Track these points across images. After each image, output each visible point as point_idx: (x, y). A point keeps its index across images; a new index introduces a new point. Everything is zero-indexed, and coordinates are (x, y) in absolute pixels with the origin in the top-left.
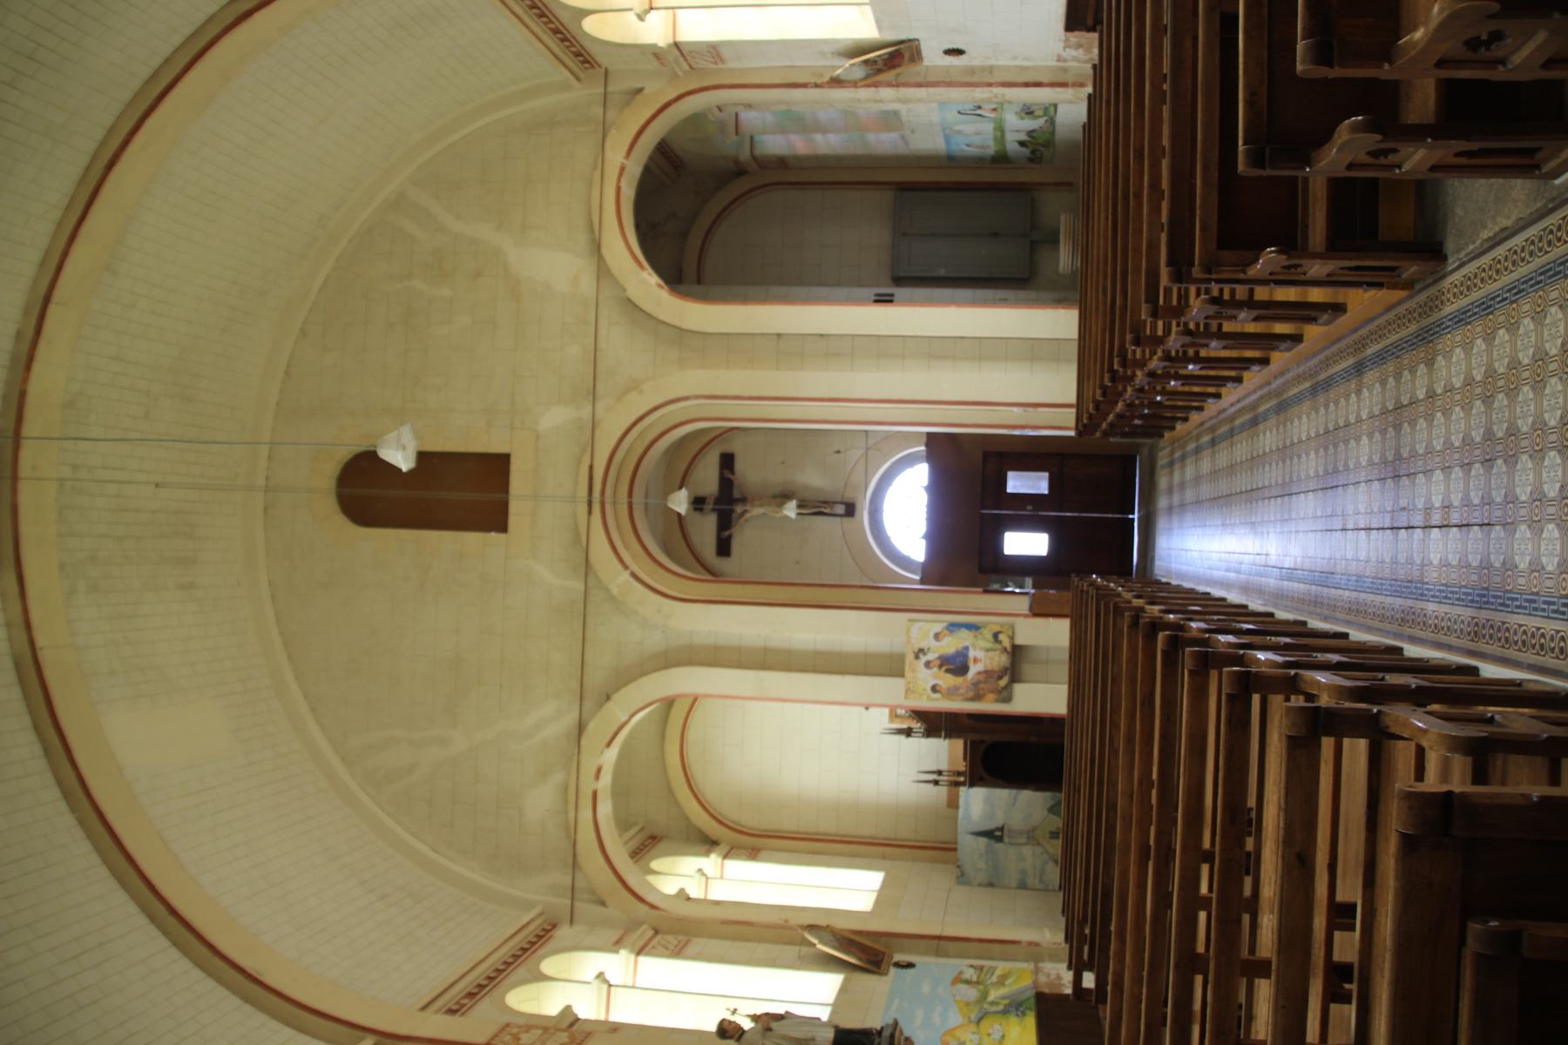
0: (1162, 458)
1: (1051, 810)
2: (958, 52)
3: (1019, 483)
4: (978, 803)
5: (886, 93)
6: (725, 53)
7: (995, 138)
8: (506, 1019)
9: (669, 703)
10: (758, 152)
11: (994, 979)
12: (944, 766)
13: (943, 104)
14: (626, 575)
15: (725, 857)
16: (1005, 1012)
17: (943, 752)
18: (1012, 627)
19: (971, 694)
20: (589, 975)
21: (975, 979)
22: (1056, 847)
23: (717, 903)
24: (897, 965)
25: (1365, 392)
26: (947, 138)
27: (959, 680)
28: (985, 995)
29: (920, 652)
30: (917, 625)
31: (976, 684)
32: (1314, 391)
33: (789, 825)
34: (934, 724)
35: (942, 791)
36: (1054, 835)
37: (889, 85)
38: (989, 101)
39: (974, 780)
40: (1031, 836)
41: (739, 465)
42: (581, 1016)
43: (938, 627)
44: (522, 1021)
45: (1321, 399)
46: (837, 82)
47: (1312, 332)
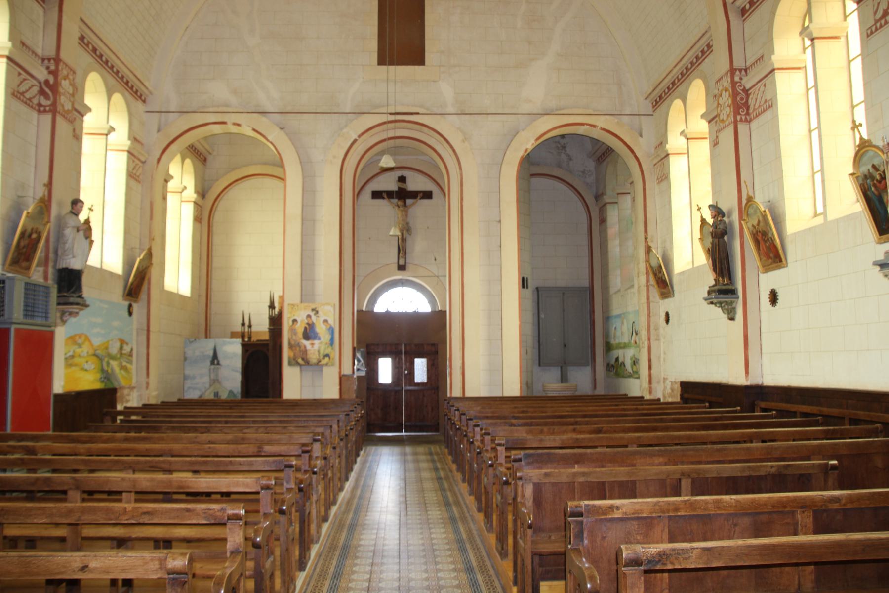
0: (434, 448)
1: (231, 392)
2: (667, 320)
3: (420, 367)
4: (233, 350)
5: (643, 279)
6: (664, 184)
7: (620, 344)
8: (79, 72)
9: (282, 165)
10: (609, 207)
11: (124, 364)
12: (254, 329)
13: (637, 313)
14: (355, 137)
15: (195, 202)
16: (102, 370)
17: (261, 327)
18: (333, 365)
19: (293, 343)
20: (112, 123)
21: (124, 352)
22: (209, 396)
23: (165, 198)
24: (130, 306)
25: (454, 574)
26: (619, 316)
27: (300, 335)
28: (113, 358)
29: (317, 312)
30: (332, 309)
31: (299, 345)
32: (460, 541)
33: (216, 239)
34: (276, 322)
35: (239, 329)
36: (216, 394)
37: (648, 281)
38: (640, 339)
39: (245, 346)
40: (215, 381)
41: (426, 202)
42: (85, 118)
43: (331, 322)
44: (78, 80)
45: (455, 546)
46: (648, 250)
47: (492, 539)
